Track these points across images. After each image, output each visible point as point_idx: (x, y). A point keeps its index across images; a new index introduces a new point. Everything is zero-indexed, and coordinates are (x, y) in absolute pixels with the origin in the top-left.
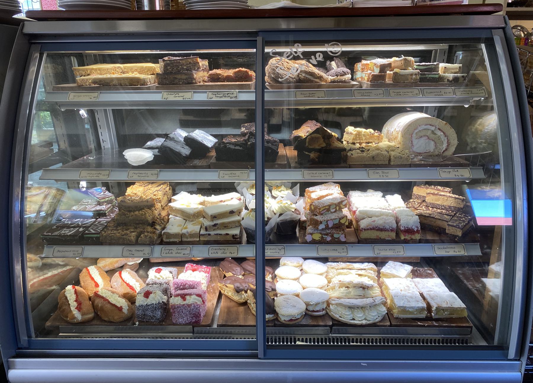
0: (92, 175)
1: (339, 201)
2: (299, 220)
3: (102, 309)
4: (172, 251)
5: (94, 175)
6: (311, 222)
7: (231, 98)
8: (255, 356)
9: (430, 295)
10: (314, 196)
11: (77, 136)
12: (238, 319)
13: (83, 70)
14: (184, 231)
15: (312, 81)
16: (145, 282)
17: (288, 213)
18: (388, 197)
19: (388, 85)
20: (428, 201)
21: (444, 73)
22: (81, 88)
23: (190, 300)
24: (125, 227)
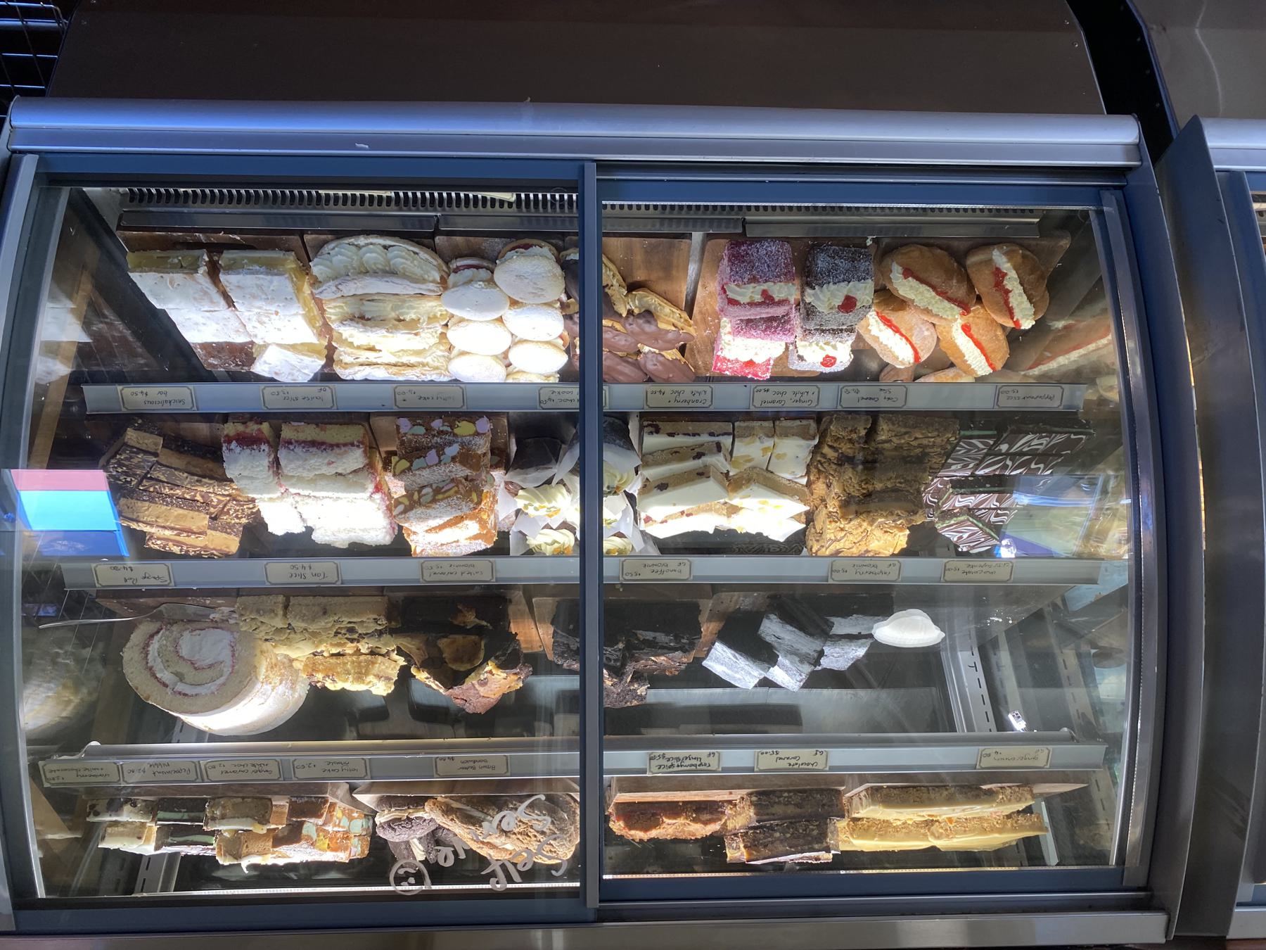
0: (985, 569)
1: (411, 514)
2: (507, 471)
3: (949, 274)
5: (979, 572)
6: (478, 462)
8: (603, 166)
9: (212, 302)
10: (472, 527)
12: (648, 252)
13: (1022, 828)
14: (769, 443)
15: (471, 802)
16: (859, 337)
17: (530, 486)
18: (298, 528)
19: (282, 790)
20: (202, 515)
21: (143, 824)
22: (1024, 779)
23: (750, 292)
24: (905, 453)
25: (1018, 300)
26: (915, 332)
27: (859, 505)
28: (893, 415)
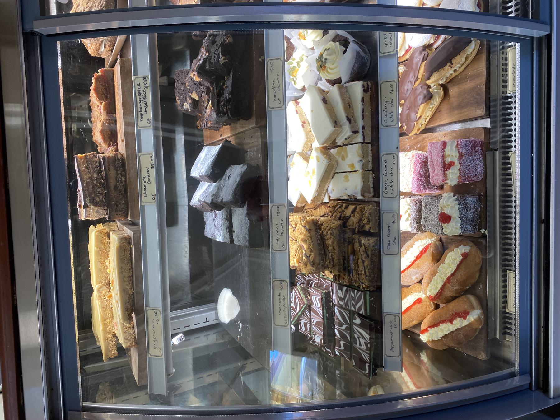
0: (282, 307)
3: (462, 283)
4: (388, 181)
7: (147, 87)
11: (196, 360)
14: (358, 167)
16: (414, 234)
22: (140, 341)
23: (452, 154)
25: (445, 329)
26: (415, 270)
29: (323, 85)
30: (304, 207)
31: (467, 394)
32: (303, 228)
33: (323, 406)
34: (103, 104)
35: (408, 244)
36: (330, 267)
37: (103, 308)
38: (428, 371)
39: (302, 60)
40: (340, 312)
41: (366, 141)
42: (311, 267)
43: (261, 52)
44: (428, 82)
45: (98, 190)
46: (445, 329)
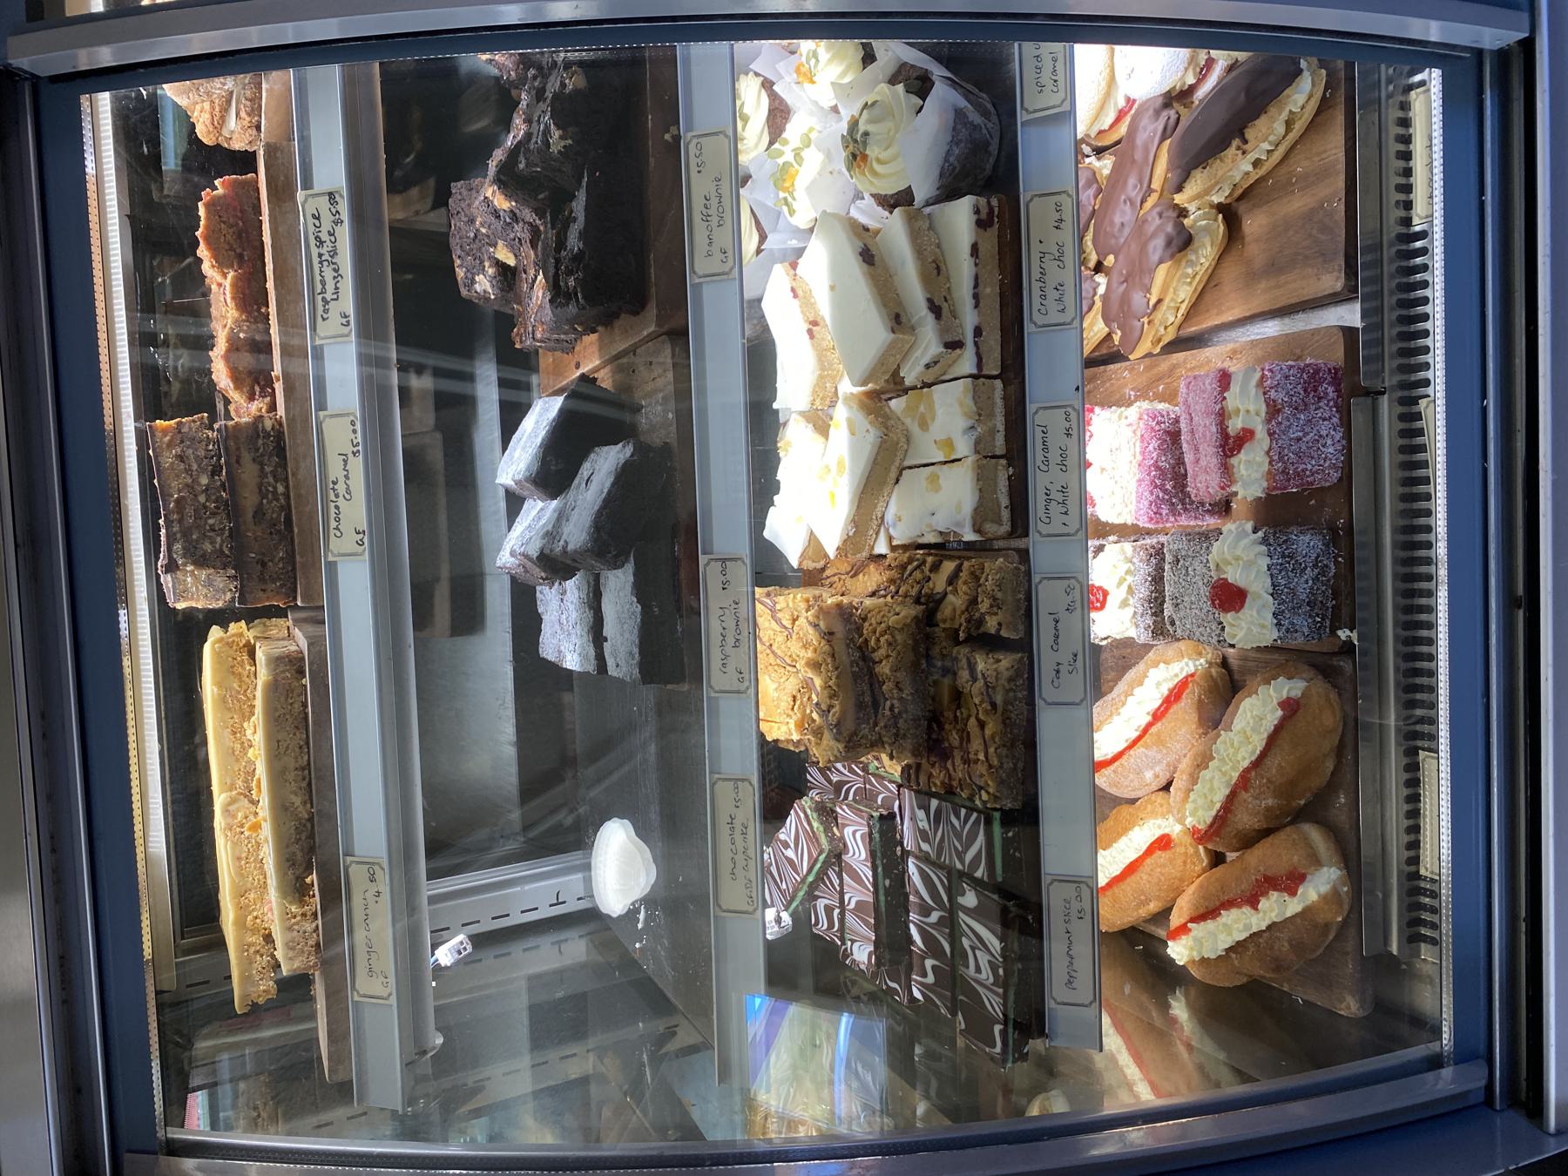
0: (740, 858)
3: (1286, 790)
4: (1054, 488)
11: (537, 1012)
14: (963, 447)
16: (1147, 648)
23: (1246, 407)
25: (1237, 924)
27: (849, 648)
28: (1027, 676)
29: (867, 213)
30: (823, 570)
31: (1301, 1116)
32: (811, 630)
33: (879, 1146)
34: (230, 276)
35: (1131, 675)
36: (891, 740)
37: (239, 859)
38: (1190, 1047)
39: (807, 142)
40: (922, 873)
41: (985, 372)
42: (833, 743)
43: (670, 112)
44: (1179, 199)
45: (211, 521)
46: (1237, 924)
